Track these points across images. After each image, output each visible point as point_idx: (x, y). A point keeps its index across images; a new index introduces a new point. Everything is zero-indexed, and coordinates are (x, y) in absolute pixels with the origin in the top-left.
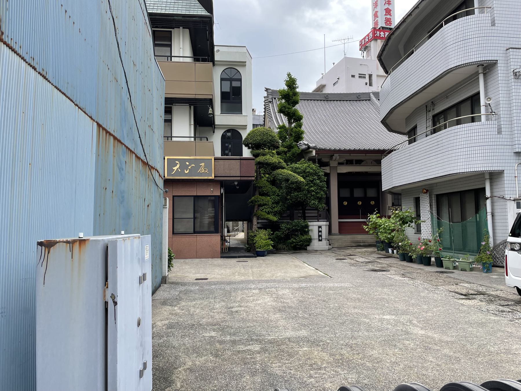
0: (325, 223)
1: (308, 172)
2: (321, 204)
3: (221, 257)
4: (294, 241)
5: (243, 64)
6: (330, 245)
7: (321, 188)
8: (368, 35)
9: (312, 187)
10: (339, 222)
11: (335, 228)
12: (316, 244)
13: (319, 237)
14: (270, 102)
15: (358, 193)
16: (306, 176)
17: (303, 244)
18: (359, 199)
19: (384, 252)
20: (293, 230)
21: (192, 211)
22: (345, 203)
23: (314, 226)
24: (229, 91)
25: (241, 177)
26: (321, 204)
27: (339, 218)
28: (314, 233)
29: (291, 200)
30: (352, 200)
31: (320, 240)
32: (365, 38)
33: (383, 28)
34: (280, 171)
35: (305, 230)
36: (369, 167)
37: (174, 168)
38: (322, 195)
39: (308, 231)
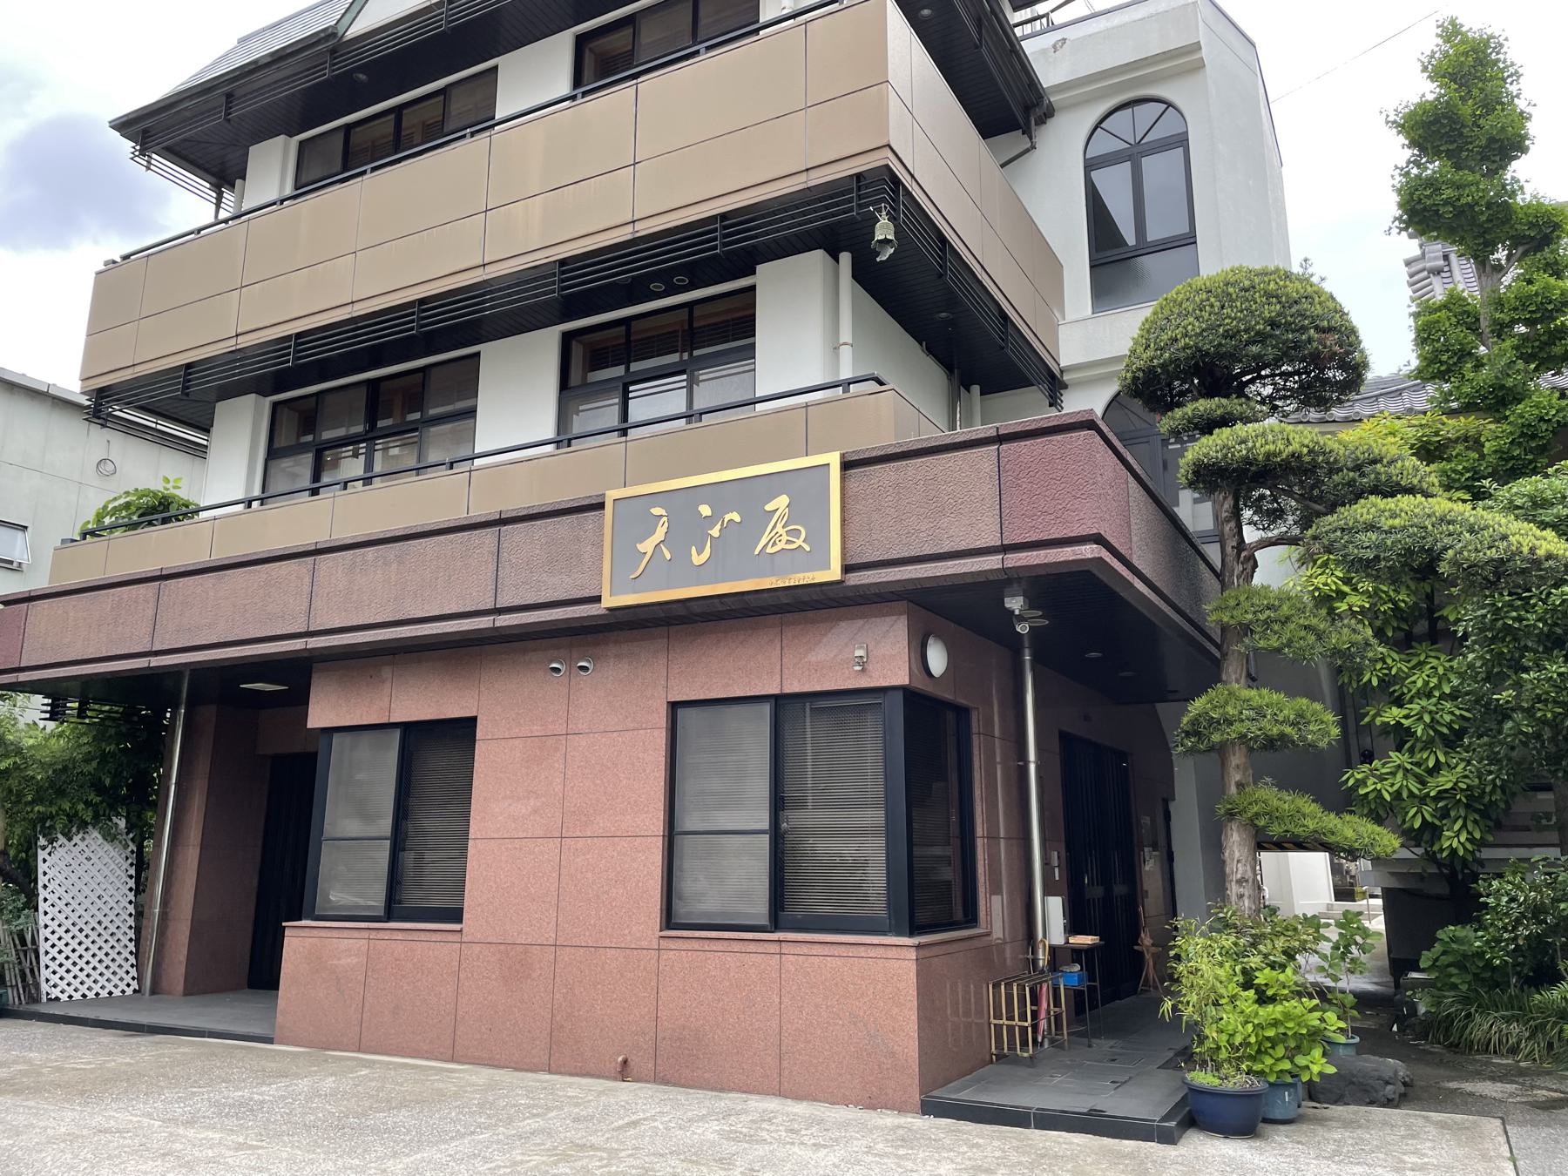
3: (932, 1108)
5: (1185, 60)
14: (1437, 272)
21: (760, 788)
25: (1005, 549)
29: (1529, 712)
34: (1367, 509)
37: (641, 547)
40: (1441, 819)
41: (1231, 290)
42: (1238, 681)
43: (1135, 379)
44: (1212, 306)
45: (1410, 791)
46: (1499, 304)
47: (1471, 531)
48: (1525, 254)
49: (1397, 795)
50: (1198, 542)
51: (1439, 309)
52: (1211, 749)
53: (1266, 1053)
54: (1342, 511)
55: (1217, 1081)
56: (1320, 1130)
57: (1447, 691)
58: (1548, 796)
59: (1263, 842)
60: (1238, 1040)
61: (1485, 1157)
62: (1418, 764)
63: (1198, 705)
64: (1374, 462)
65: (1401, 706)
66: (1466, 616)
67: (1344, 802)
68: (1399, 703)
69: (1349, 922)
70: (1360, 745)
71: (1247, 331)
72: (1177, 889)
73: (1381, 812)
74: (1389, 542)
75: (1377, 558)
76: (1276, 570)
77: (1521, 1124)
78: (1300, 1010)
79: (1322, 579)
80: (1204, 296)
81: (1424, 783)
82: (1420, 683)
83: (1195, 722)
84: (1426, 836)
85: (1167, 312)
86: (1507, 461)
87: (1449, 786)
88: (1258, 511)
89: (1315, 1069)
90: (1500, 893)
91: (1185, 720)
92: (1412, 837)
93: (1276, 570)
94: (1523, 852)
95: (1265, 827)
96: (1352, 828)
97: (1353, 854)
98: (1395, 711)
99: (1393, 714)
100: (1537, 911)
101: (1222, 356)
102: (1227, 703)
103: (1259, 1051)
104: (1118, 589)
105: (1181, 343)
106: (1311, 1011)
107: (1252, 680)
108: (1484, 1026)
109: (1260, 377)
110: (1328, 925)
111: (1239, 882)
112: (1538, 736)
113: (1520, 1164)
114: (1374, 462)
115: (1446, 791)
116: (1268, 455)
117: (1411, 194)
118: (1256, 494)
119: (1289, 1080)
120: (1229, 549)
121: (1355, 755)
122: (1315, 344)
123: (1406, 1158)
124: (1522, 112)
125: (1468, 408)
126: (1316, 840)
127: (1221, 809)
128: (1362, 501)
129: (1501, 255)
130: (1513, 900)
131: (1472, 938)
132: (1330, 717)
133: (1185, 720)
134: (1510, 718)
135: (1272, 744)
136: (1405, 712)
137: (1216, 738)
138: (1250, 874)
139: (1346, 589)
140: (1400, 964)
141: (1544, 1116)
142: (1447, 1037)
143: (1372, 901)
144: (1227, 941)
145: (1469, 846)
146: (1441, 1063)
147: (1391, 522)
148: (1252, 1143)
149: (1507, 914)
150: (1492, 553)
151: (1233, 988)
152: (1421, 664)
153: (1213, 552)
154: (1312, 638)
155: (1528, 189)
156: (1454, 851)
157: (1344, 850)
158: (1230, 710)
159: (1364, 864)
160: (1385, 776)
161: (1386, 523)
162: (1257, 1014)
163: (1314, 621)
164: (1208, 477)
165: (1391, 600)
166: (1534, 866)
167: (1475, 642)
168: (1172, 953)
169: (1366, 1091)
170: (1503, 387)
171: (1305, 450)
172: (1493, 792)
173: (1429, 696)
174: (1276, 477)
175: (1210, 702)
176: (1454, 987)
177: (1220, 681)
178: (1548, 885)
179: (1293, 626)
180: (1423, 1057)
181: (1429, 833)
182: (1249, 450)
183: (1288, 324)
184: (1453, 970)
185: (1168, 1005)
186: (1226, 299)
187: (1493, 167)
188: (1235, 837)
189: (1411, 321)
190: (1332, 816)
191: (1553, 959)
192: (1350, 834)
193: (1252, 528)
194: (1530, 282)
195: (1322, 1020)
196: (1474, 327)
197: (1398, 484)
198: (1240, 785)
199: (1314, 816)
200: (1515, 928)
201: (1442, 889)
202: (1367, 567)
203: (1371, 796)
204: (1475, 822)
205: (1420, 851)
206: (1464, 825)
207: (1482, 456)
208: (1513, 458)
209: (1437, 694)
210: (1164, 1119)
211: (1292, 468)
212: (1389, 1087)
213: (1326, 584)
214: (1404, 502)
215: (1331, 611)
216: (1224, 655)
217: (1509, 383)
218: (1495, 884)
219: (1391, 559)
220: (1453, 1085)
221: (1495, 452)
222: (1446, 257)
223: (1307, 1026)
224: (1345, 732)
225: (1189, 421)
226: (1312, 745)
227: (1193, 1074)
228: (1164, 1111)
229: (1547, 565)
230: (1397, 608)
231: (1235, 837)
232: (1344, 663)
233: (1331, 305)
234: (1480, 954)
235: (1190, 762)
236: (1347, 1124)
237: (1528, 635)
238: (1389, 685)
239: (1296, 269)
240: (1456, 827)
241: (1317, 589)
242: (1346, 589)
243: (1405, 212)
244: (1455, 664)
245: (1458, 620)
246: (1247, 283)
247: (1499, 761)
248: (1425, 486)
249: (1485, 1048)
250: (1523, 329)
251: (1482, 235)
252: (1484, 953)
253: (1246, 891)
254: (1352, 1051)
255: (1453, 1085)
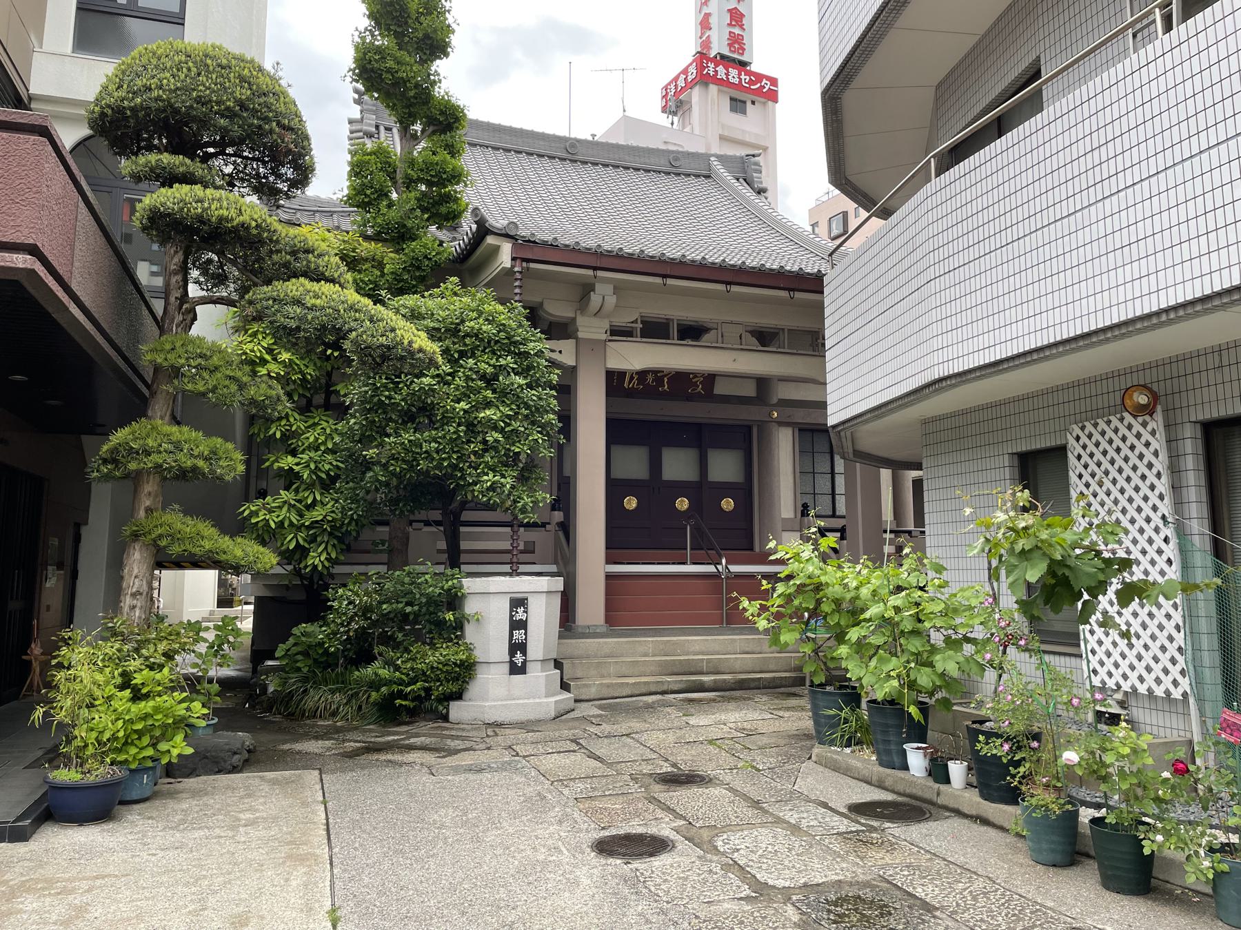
0: (543, 583)
1: (476, 335)
2: (532, 490)
4: (384, 673)
6: (565, 686)
7: (533, 415)
8: (685, 71)
9: (488, 404)
10: (609, 577)
11: (591, 605)
12: (494, 694)
13: (512, 653)
15: (678, 465)
16: (463, 354)
17: (428, 691)
18: (680, 488)
19: (865, 759)
20: (386, 618)
22: (631, 503)
23: (488, 598)
24: (186, 40)
26: (532, 490)
27: (609, 561)
28: (487, 635)
29: (385, 466)
30: (655, 490)
31: (517, 669)
32: (676, 79)
33: (723, 57)
34: (296, 287)
35: (442, 618)
36: (734, 354)
38: (534, 446)
39: (459, 625)
40: (309, 543)
41: (209, 62)
42: (162, 418)
43: (103, 115)
44: (189, 70)
45: (291, 521)
46: (412, 163)
47: (371, 321)
48: (434, 133)
49: (280, 524)
50: (147, 295)
51: (370, 154)
52: (127, 476)
53: (132, 743)
54: (278, 284)
55: (79, 776)
56: (171, 804)
57: (330, 446)
58: (386, 529)
59: (164, 561)
60: (107, 735)
61: (305, 804)
62: (299, 501)
63: (120, 436)
64: (307, 251)
65: (294, 456)
66: (353, 391)
67: (236, 527)
68: (294, 453)
69: (227, 627)
70: (257, 483)
71: (218, 103)
72: (77, 603)
73: (267, 538)
74: (309, 317)
75: (298, 328)
76: (212, 324)
77: (333, 772)
78: (170, 702)
79: (250, 346)
80: (183, 58)
81: (301, 516)
82: (312, 439)
83: (115, 450)
84: (297, 556)
85: (144, 61)
86: (399, 281)
87: (320, 518)
88: (205, 272)
89: (175, 752)
90: (344, 599)
91: (105, 448)
92: (287, 556)
93: (212, 324)
94: (362, 569)
95: (165, 547)
96: (241, 548)
97: (237, 570)
98: (290, 459)
99: (288, 461)
100: (366, 611)
101: (194, 119)
102: (148, 436)
103: (126, 743)
104: (50, 310)
105: (155, 94)
106: (180, 702)
107: (176, 421)
108: (317, 697)
109: (223, 153)
110: (207, 629)
111: (134, 595)
112: (387, 484)
113: (330, 805)
114: (307, 251)
115: (317, 522)
116: (221, 219)
117: (365, 54)
118: (205, 257)
119: (150, 764)
120: (172, 299)
121: (252, 493)
122: (275, 137)
123: (242, 816)
124: (449, 26)
125: (376, 238)
126: (209, 558)
127: (127, 530)
128: (294, 280)
129: (418, 127)
130: (350, 603)
131: (314, 632)
132: (239, 456)
133: (105, 448)
134: (370, 469)
135: (184, 475)
136: (297, 460)
137: (133, 466)
138: (145, 588)
139: (268, 357)
140: (260, 653)
141: (350, 762)
142: (287, 707)
143: (246, 607)
144: (111, 647)
145: (326, 564)
146: (281, 730)
147: (313, 301)
148: (105, 826)
149: (345, 614)
150: (383, 340)
151: (110, 690)
152: (315, 424)
153: (158, 306)
154: (234, 388)
155: (444, 85)
156: (315, 567)
157: (232, 567)
158: (150, 442)
159: (246, 578)
160: (274, 509)
161: (310, 301)
162: (129, 711)
163: (239, 374)
164: (165, 226)
165: (301, 372)
166: (369, 578)
167: (356, 411)
168: (54, 662)
169: (217, 763)
170: (404, 226)
171: (254, 224)
172: (349, 523)
173: (317, 449)
174: (225, 242)
175: (133, 433)
176: (299, 669)
177: (145, 416)
178: (376, 592)
179: (219, 375)
180: (266, 726)
181: (302, 551)
182: (204, 210)
183: (255, 111)
184: (300, 657)
185: (39, 712)
186: (202, 68)
187: (424, 57)
188: (137, 555)
189: (349, 157)
190: (227, 538)
191: (371, 646)
192: (239, 553)
193: (196, 287)
194: (434, 154)
195: (188, 709)
196: (392, 176)
197: (323, 274)
198: (149, 510)
199: (210, 537)
200: (349, 623)
201: (301, 596)
202: (289, 334)
203: (260, 525)
204: (334, 546)
205: (289, 568)
206: (326, 548)
207: (383, 275)
208: (403, 280)
209: (322, 448)
210: (19, 819)
211: (240, 238)
212: (237, 757)
213: (252, 351)
214: (326, 288)
215: (254, 373)
216: (153, 394)
217: (409, 224)
218: (340, 591)
219: (309, 331)
220: (286, 747)
221: (392, 273)
222: (377, 127)
223: (174, 716)
224: (248, 470)
225: (152, 170)
226: (220, 478)
227: (56, 773)
228: (20, 811)
229: (418, 356)
230: (304, 380)
231: (137, 555)
232: (257, 415)
233: (294, 109)
234: (321, 644)
235: (107, 487)
236: (195, 794)
237: (393, 410)
238: (288, 438)
239: (268, 66)
240: (320, 550)
241: (245, 353)
242: (268, 357)
243: (358, 67)
244: (339, 427)
245: (345, 395)
246: (224, 62)
247: (358, 501)
248: (342, 281)
249: (314, 715)
250: (423, 188)
251: (408, 107)
252: (324, 643)
253: (139, 603)
254: (210, 731)
255: (286, 747)
